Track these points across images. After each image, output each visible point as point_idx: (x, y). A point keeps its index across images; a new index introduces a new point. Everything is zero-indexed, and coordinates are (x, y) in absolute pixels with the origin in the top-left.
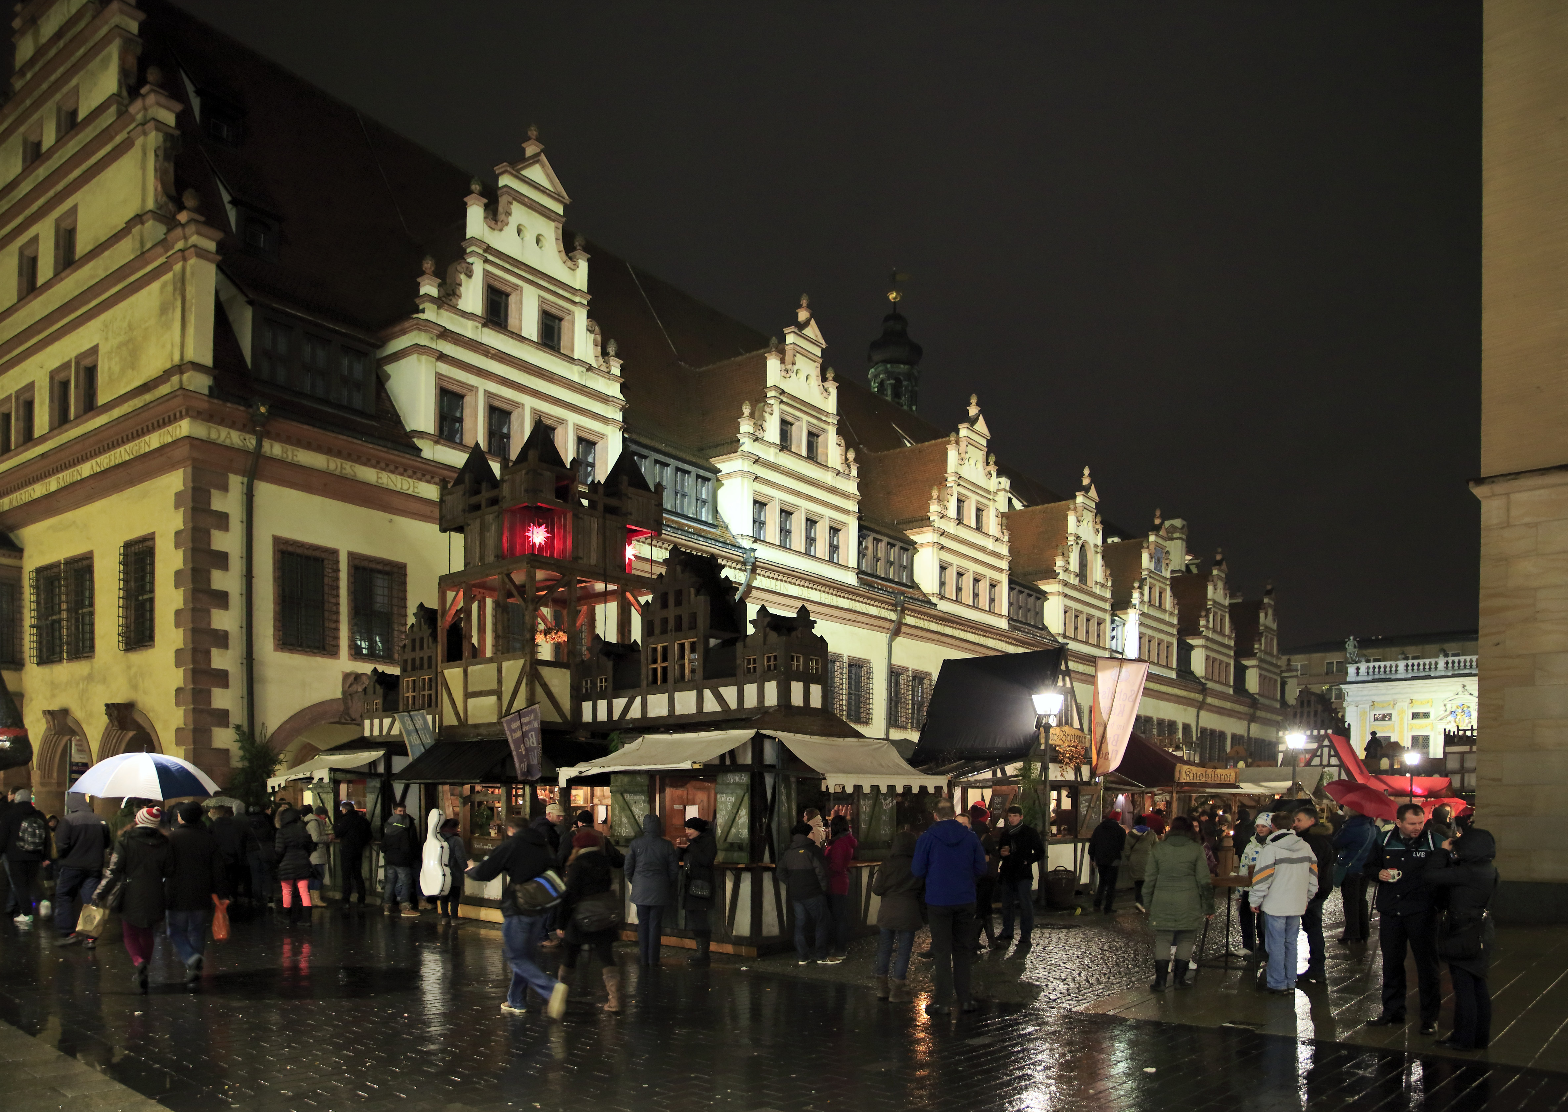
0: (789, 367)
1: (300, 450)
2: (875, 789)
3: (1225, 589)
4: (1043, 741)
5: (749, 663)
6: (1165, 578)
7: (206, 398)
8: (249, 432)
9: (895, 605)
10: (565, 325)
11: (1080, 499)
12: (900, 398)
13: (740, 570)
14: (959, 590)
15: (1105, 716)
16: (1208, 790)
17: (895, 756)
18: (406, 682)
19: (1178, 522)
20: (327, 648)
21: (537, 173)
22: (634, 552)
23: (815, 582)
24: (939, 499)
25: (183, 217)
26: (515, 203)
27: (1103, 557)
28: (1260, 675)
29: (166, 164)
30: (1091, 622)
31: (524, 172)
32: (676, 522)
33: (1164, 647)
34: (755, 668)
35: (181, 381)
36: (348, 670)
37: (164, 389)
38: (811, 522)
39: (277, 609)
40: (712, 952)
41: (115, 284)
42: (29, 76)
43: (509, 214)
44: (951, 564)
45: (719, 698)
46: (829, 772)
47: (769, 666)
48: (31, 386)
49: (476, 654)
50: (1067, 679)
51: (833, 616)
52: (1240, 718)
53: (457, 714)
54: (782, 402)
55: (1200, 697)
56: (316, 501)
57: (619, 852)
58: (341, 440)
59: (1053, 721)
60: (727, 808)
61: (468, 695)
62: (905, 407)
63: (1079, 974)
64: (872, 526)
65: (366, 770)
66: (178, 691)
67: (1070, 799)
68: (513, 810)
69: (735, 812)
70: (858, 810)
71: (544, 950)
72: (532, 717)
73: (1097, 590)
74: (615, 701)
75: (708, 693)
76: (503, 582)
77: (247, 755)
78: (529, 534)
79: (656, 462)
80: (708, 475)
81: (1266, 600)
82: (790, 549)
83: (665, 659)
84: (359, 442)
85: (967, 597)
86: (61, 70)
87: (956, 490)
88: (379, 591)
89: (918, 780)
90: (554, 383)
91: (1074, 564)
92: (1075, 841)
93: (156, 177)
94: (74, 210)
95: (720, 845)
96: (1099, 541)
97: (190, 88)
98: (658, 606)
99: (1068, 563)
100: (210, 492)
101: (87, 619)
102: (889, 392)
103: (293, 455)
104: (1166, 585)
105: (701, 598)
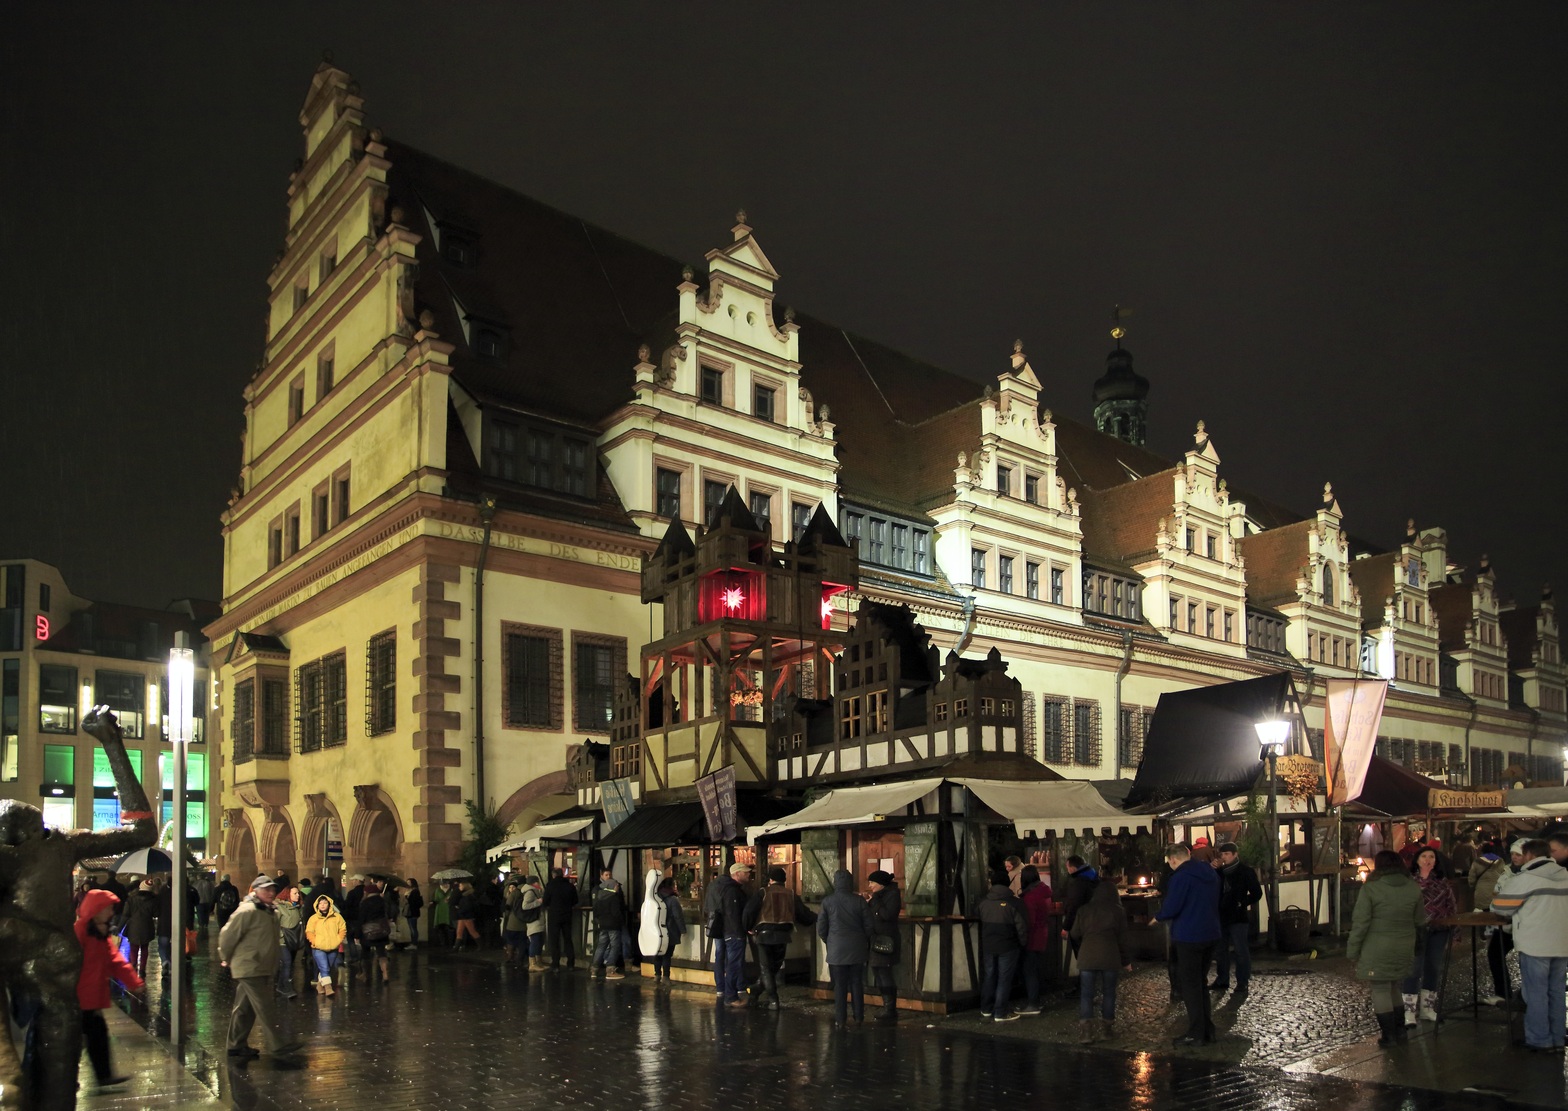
0: (1004, 413)
1: (526, 538)
2: (1070, 832)
3: (1493, 597)
4: (1268, 772)
5: (939, 711)
6: (1423, 592)
7: (439, 498)
8: (478, 526)
9: (1123, 642)
10: (777, 395)
11: (1322, 516)
12: (1128, 434)
13: (960, 619)
14: (1192, 621)
15: (1338, 742)
16: (1468, 816)
17: (1095, 795)
18: (616, 751)
19: (1436, 532)
20: (551, 723)
21: (747, 255)
22: (831, 608)
23: (1037, 625)
24: (1167, 531)
25: (419, 336)
26: (725, 285)
27: (1350, 575)
28: (1541, 687)
29: (407, 291)
30: (1339, 644)
31: (733, 256)
32: (894, 577)
33: (1423, 664)
34: (945, 715)
35: (418, 485)
36: (572, 743)
37: (404, 494)
38: (1032, 566)
39: (505, 689)
40: (901, 1009)
41: (365, 404)
42: (300, 233)
43: (720, 296)
44: (1182, 596)
45: (911, 748)
46: (1018, 817)
47: (959, 712)
48: (297, 504)
49: (677, 718)
50: (1295, 705)
51: (1058, 659)
52: (1518, 736)
53: (658, 779)
54: (998, 448)
55: (1469, 716)
56: (541, 585)
57: (808, 909)
58: (562, 525)
59: (1280, 751)
60: (914, 859)
61: (668, 760)
62: (1133, 443)
63: (1298, 1027)
64: (1097, 564)
65: (577, 838)
66: (416, 771)
67: (1303, 833)
68: (709, 870)
69: (922, 863)
70: (1057, 856)
71: (733, 1011)
72: (727, 778)
73: (1345, 610)
74: (810, 757)
75: (899, 744)
76: (700, 647)
77: (477, 828)
78: (724, 598)
79: (872, 519)
80: (925, 527)
81: (1544, 606)
82: (1011, 594)
83: (857, 712)
84: (581, 526)
85: (1201, 628)
86: (325, 223)
87: (1185, 519)
88: (601, 665)
89: (1134, 822)
90: (767, 452)
91: (1318, 585)
92: (1310, 878)
93: (398, 304)
94: (332, 344)
95: (905, 898)
96: (1345, 558)
97: (431, 221)
98: (850, 659)
99: (1311, 585)
100: (443, 584)
101: (341, 710)
102: (1116, 429)
103: (519, 544)
104: (1424, 598)
105: (891, 648)
